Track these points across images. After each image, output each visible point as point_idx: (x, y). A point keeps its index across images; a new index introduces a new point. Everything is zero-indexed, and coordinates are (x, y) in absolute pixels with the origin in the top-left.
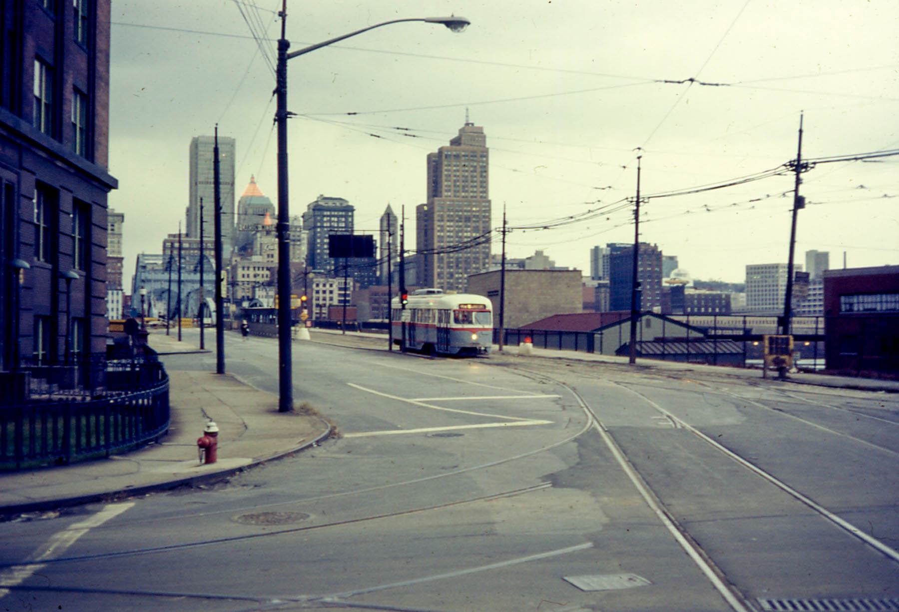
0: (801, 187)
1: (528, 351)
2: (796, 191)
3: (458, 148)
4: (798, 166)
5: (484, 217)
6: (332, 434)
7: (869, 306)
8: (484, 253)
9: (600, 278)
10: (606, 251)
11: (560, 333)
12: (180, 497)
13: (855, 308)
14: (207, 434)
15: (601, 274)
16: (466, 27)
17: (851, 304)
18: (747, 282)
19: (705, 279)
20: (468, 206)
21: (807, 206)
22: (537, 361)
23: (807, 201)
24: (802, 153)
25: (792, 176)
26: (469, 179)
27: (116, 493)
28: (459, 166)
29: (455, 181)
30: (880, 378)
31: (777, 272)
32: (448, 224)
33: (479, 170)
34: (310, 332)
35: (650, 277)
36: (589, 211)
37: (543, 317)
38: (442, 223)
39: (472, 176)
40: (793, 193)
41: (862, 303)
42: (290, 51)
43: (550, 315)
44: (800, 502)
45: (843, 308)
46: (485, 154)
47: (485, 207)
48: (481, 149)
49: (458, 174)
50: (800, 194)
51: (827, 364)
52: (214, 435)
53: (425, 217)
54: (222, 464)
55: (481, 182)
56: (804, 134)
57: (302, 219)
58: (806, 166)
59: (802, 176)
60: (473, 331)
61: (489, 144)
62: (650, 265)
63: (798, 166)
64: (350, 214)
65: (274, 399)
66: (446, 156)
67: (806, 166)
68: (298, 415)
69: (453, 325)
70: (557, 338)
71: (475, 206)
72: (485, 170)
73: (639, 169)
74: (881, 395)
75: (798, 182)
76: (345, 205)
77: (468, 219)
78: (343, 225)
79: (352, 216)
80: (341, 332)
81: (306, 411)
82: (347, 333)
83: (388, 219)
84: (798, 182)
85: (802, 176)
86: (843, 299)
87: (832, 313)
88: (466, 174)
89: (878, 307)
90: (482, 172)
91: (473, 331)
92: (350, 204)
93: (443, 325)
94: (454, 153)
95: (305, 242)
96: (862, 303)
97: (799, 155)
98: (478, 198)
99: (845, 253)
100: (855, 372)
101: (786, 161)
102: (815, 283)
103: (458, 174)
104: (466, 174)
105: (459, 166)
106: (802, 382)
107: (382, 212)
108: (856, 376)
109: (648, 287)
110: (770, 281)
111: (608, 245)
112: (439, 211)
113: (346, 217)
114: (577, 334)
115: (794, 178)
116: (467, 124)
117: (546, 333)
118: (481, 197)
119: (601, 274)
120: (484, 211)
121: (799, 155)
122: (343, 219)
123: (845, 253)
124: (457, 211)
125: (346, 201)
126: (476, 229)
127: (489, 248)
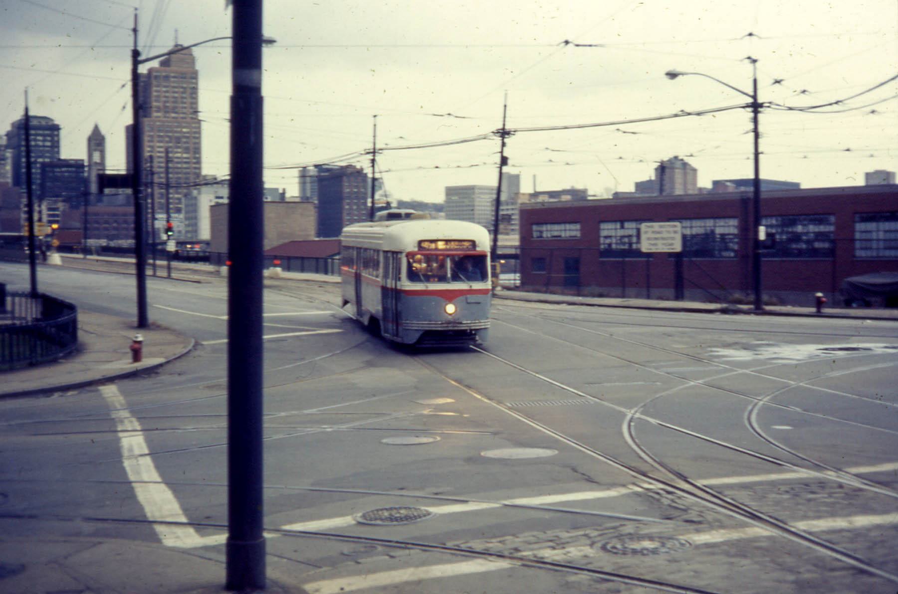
0: (505, 149)
1: (277, 274)
2: (502, 152)
3: (167, 69)
4: (504, 133)
5: (195, 138)
6: (197, 345)
7: (556, 234)
8: (195, 173)
10: (312, 171)
11: (303, 258)
12: (48, 399)
13: (544, 235)
14: (136, 342)
16: (275, 44)
17: (541, 232)
18: (446, 202)
19: (406, 198)
20: (177, 127)
22: (290, 283)
25: (498, 140)
26: (179, 100)
27: (100, 380)
29: (165, 102)
30: (563, 294)
31: (474, 193)
32: (158, 144)
33: (189, 91)
34: (62, 257)
35: (357, 198)
38: (151, 144)
39: (183, 98)
40: (499, 155)
41: (550, 231)
42: (140, 58)
43: (286, 241)
44: (395, 539)
45: (535, 234)
46: (194, 76)
47: (195, 128)
49: (167, 94)
50: (505, 154)
51: (522, 279)
52: (140, 342)
53: (135, 135)
54: (147, 362)
55: (192, 103)
56: (508, 108)
57: (5, 138)
58: (508, 133)
59: (506, 140)
60: (450, 296)
61: (198, 66)
62: (357, 187)
63: (504, 133)
64: (56, 133)
65: (135, 320)
66: (156, 77)
67: (508, 133)
68: (153, 330)
69: (407, 285)
70: (299, 262)
71: (185, 127)
72: (194, 91)
74: (564, 306)
75: (504, 145)
76: (50, 123)
77: (178, 140)
78: (48, 144)
79: (58, 135)
80: (81, 256)
81: (158, 327)
82: (89, 257)
83: (97, 141)
84: (504, 145)
85: (506, 140)
86: (535, 228)
87: (526, 237)
88: (176, 95)
89: (563, 234)
90: (191, 94)
91: (450, 296)
92: (56, 122)
93: (390, 284)
94: (164, 74)
95: (9, 161)
96: (550, 231)
98: (188, 120)
99: (534, 176)
100: (544, 289)
101: (494, 129)
102: (507, 204)
103: (167, 94)
104: (176, 95)
106: (506, 298)
107: (88, 131)
108: (546, 292)
109: (355, 207)
110: (467, 202)
111: (316, 166)
112: (149, 131)
113: (52, 136)
114: (317, 259)
117: (289, 258)
118: (192, 118)
119: (308, 194)
120: (195, 133)
122: (49, 138)
123: (534, 176)
124: (167, 132)
125: (52, 120)
126: (187, 150)
127: (199, 168)
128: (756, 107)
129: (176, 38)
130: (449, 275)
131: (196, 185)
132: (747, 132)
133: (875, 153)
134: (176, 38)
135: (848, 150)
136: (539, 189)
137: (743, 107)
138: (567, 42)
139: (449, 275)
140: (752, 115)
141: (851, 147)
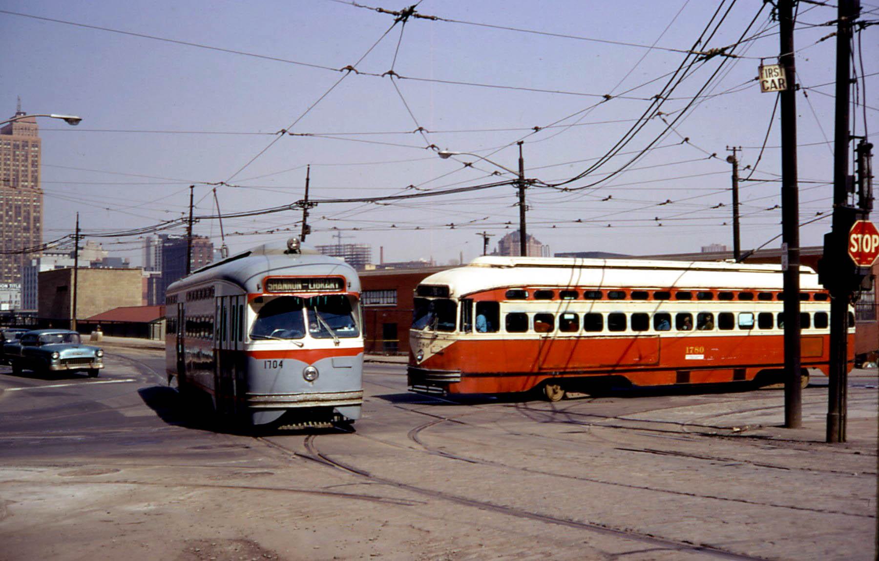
0: (308, 219)
4: (306, 204)
9: (152, 269)
15: (153, 264)
21: (312, 233)
23: (312, 229)
24: (309, 194)
28: (82, 248)
36: (818, 214)
37: (107, 310)
43: (113, 307)
48: (34, 138)
58: (311, 205)
59: (308, 211)
63: (306, 204)
73: (823, 40)
75: (306, 215)
84: (306, 215)
97: (306, 197)
105: (82, 248)
108: (373, 354)
115: (302, 212)
116: (19, 113)
121: (306, 197)
128: (522, 184)
129: (19, 106)
130: (154, 303)
131: (36, 250)
132: (514, 205)
133: (556, 225)
134: (19, 106)
135: (579, 221)
136: (386, 261)
137: (511, 184)
138: (284, 132)
139: (154, 303)
140: (518, 190)
141: (582, 219)
